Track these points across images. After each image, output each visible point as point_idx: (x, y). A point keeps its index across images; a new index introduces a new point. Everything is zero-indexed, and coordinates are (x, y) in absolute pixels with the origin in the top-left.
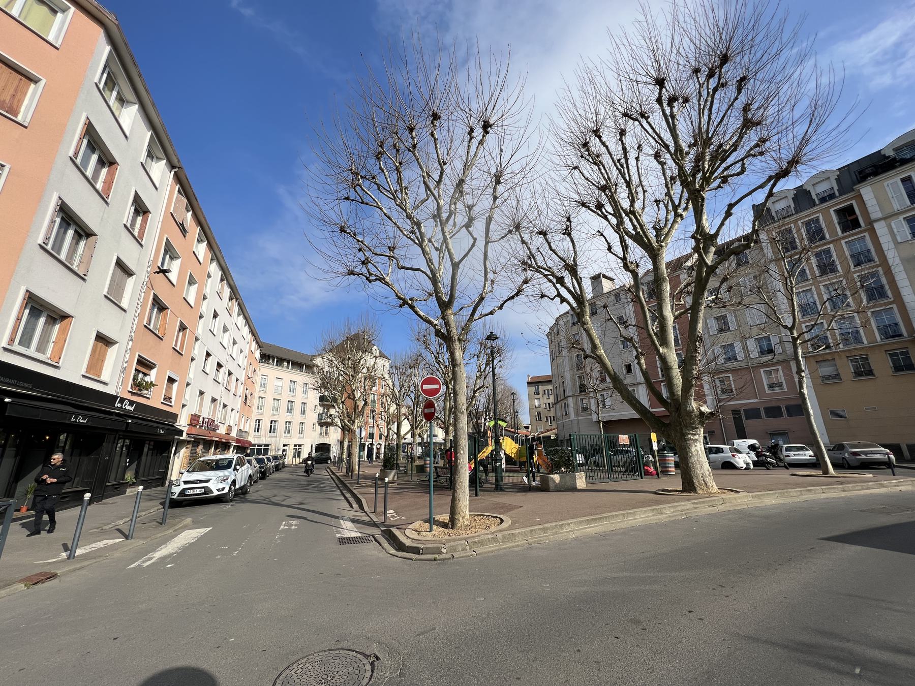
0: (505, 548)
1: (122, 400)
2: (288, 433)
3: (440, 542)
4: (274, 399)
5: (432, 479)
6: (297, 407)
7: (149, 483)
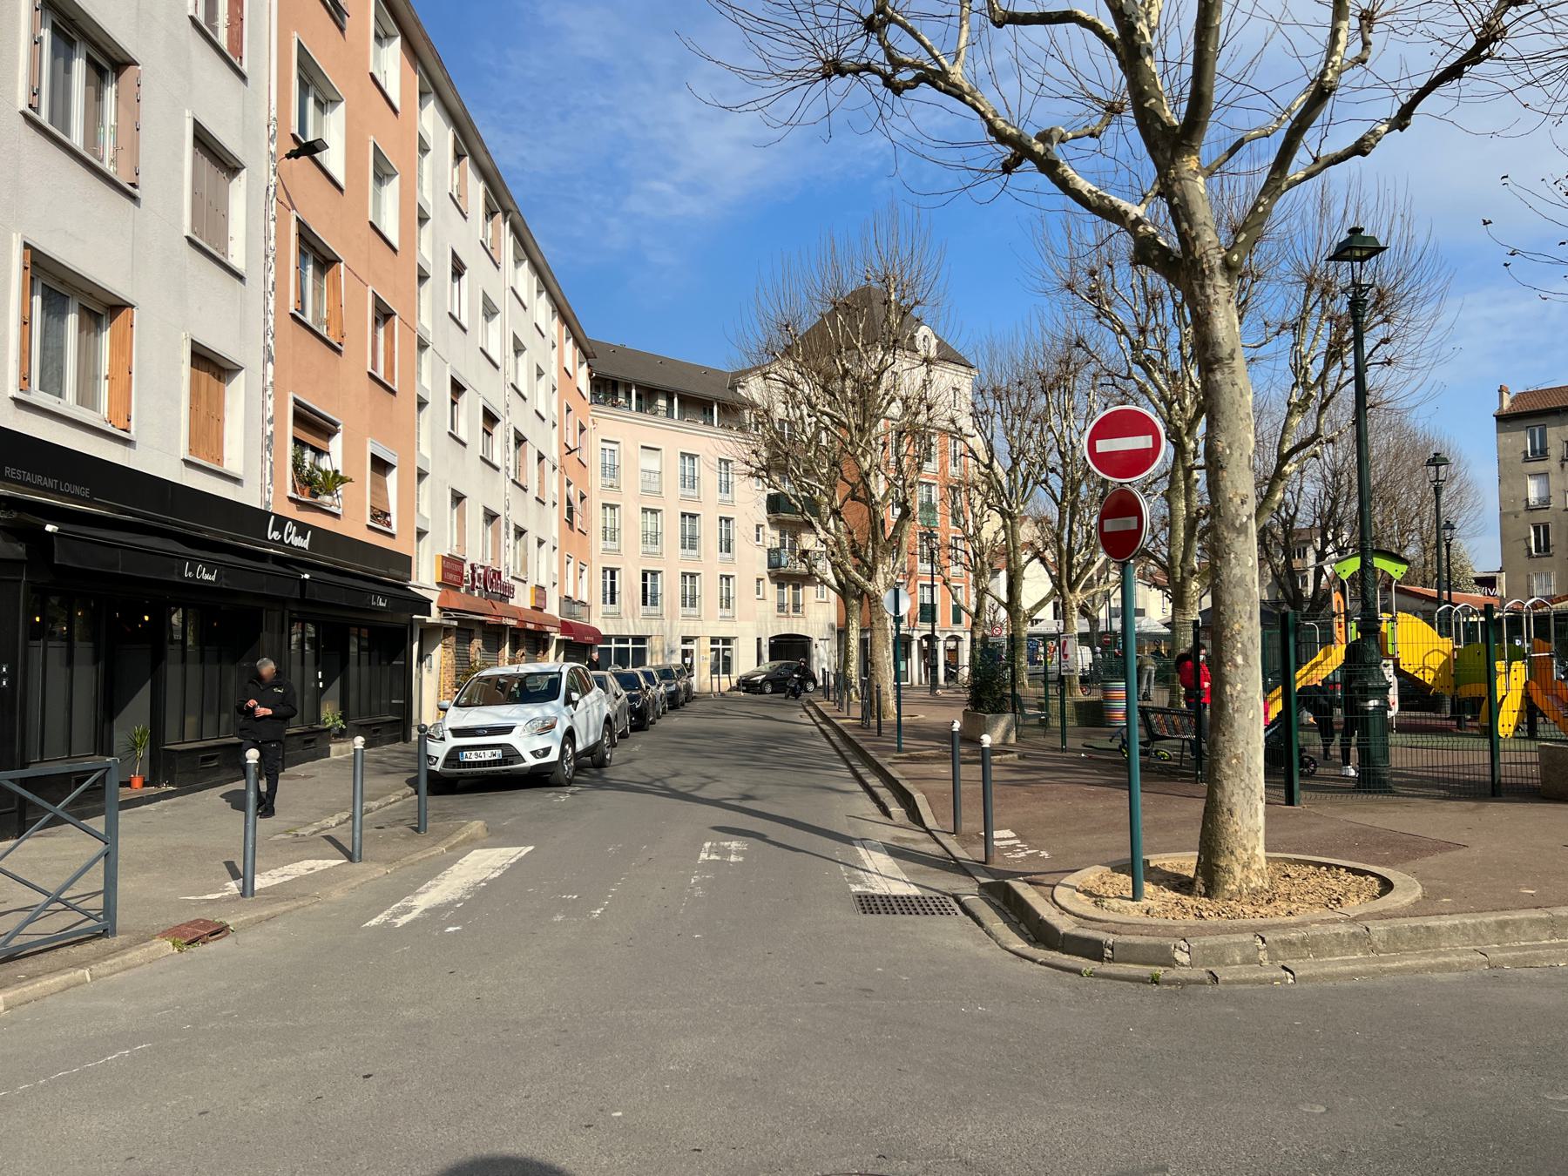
0: (1398, 970)
1: (281, 522)
2: (693, 605)
3: (1169, 931)
4: (645, 510)
5: (1136, 748)
6: (709, 532)
7: (376, 731)
